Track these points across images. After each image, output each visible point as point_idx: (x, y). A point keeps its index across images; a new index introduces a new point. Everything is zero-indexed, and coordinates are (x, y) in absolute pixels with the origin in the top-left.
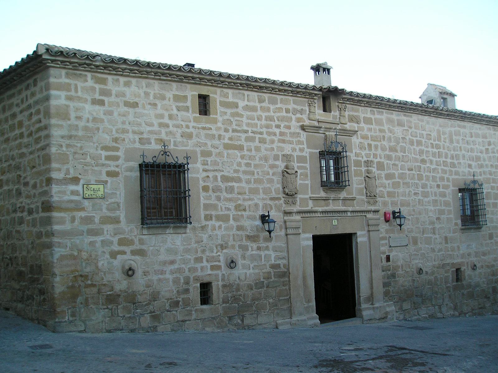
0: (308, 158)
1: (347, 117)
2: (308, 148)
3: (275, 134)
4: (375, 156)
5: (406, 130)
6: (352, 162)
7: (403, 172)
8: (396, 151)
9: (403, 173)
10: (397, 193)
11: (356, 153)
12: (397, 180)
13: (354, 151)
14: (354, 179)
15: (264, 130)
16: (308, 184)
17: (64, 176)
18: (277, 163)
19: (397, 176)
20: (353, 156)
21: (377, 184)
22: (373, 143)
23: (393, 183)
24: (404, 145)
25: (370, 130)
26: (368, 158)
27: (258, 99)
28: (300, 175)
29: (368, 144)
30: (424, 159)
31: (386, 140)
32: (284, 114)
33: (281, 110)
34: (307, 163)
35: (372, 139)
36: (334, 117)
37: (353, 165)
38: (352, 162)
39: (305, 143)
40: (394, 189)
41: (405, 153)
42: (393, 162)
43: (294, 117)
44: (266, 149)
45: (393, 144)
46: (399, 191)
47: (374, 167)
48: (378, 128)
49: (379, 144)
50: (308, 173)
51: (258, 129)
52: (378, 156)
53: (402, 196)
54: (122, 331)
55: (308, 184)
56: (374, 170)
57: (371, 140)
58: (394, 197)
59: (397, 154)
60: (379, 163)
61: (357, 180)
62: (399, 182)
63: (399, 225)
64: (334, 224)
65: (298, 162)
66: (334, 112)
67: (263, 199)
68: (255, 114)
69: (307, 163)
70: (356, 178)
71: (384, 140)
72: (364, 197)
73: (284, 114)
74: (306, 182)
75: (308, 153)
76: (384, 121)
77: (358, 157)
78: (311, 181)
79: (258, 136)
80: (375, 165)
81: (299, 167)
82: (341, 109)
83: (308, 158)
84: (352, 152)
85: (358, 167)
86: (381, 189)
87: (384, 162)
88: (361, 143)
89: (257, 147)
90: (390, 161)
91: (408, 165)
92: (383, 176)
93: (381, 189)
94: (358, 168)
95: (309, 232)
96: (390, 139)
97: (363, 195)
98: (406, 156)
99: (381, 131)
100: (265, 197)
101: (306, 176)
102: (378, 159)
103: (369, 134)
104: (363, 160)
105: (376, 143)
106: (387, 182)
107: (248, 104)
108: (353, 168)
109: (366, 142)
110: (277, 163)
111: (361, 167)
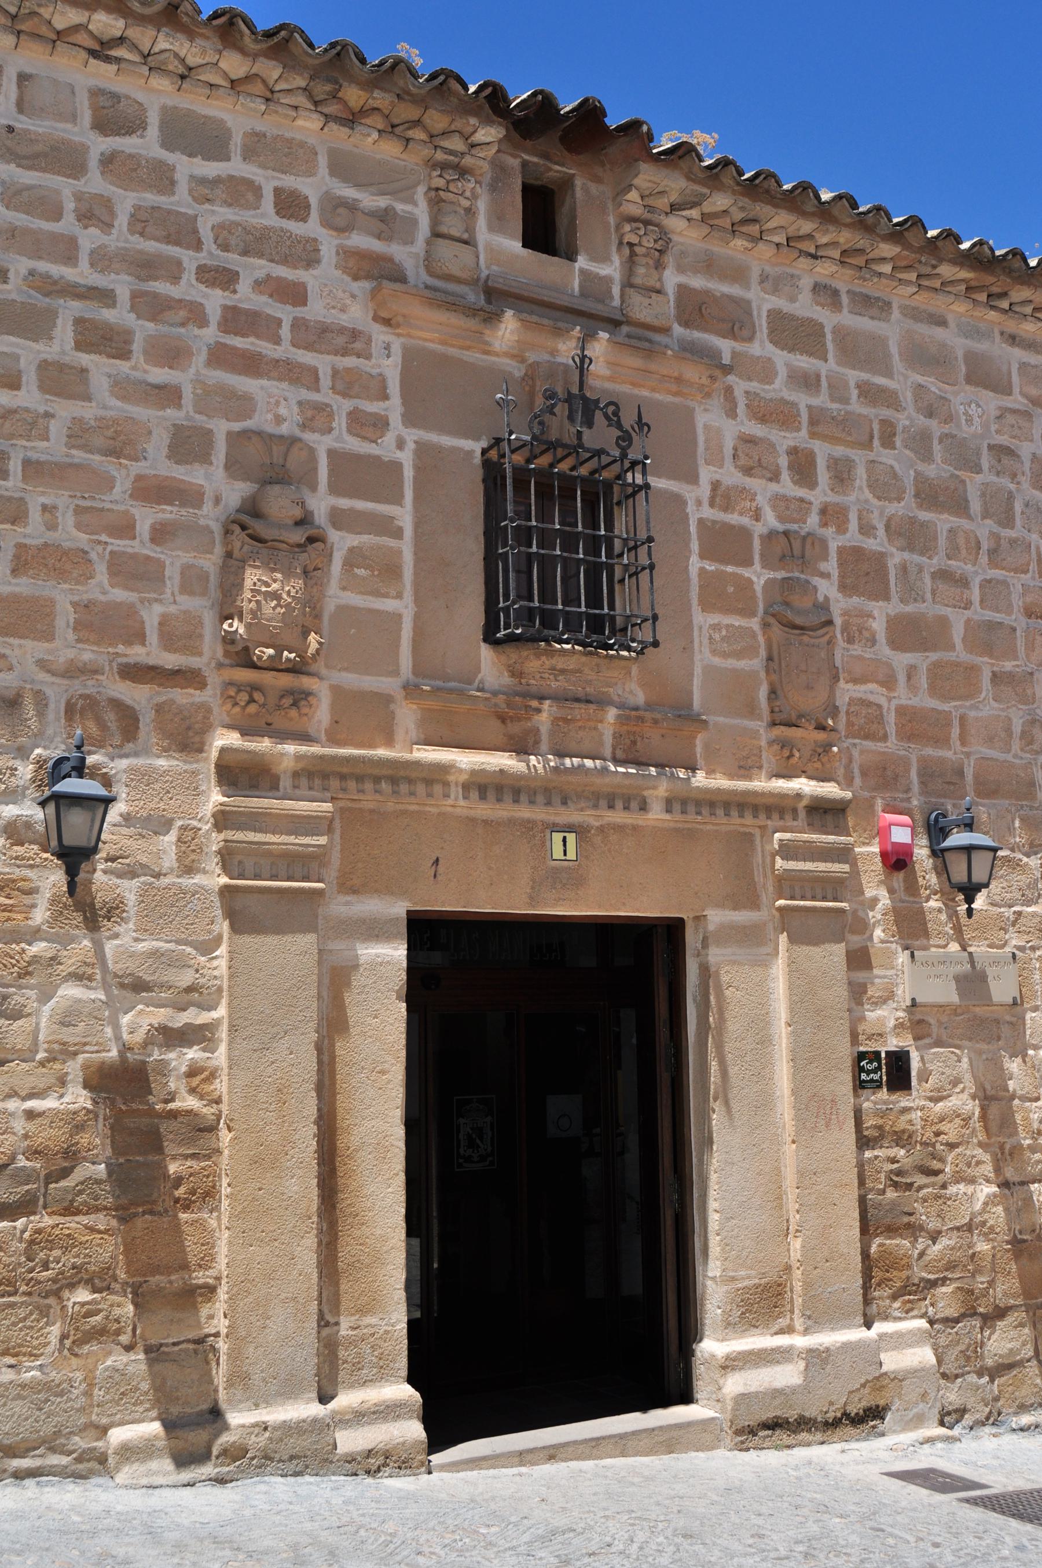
0: (408, 473)
1: (672, 298)
2: (410, 419)
3: (197, 315)
4: (833, 515)
5: (1014, 411)
6: (693, 529)
7: (998, 617)
8: (961, 507)
9: (992, 626)
10: (956, 723)
11: (715, 486)
12: (960, 654)
13: (706, 474)
14: (702, 619)
15: (122, 285)
16: (396, 618)
17: (523, 462)
18: (194, 475)
19: (957, 633)
20: (699, 503)
21: (838, 663)
22: (822, 451)
23: (935, 669)
24: (1005, 482)
25: (808, 382)
26: (794, 521)
27: (96, 109)
28: (349, 564)
29: (826, 361)
30: (795, 483)
31: (898, 441)
32: (266, 216)
33: (250, 196)
34: (398, 501)
35: (819, 429)
36: (593, 286)
37: (695, 546)
38: (693, 529)
39: (394, 387)
40: (945, 698)
41: (1008, 521)
42: (937, 562)
43: (328, 244)
44: (123, 388)
45: (937, 469)
46: (973, 714)
47: (826, 576)
48: (854, 376)
49: (858, 456)
50: (400, 552)
51: (82, 273)
52: (853, 517)
53: (990, 740)
54: (943, 395)
55: (396, 618)
56: (827, 589)
57: (813, 435)
58: (943, 741)
59: (964, 523)
60: (852, 557)
61: (716, 627)
62: (973, 670)
63: (961, 889)
64: (571, 838)
65: (335, 489)
66: (593, 259)
67: (74, 671)
68: (64, 187)
69: (398, 501)
70: (715, 618)
71: (888, 442)
72: (759, 726)
73: (266, 216)
74: (389, 605)
75: (411, 446)
76: (894, 350)
77: (726, 508)
78: (417, 600)
79: (70, 309)
80: (831, 566)
81: (339, 519)
82: (637, 249)
83: (408, 473)
84: (693, 478)
85: (727, 563)
86: (871, 691)
87: (882, 555)
88: (749, 440)
89: (62, 367)
90: (922, 554)
91: (1026, 589)
92: (878, 626)
93: (871, 691)
94: (730, 569)
95: (388, 889)
96: (921, 444)
97: (751, 710)
98: (1013, 542)
99: (869, 393)
100: (87, 655)
101: (391, 571)
102: (852, 536)
103: (803, 400)
104: (759, 529)
105: (839, 451)
106: (902, 660)
107: (17, 125)
108: (695, 564)
109: (783, 440)
110: (194, 475)
111: (748, 562)
